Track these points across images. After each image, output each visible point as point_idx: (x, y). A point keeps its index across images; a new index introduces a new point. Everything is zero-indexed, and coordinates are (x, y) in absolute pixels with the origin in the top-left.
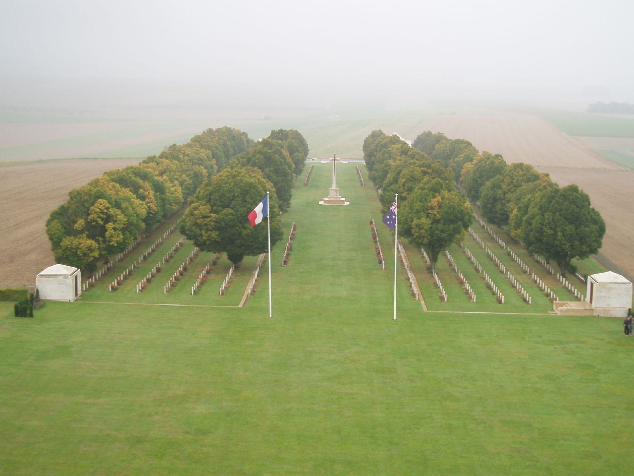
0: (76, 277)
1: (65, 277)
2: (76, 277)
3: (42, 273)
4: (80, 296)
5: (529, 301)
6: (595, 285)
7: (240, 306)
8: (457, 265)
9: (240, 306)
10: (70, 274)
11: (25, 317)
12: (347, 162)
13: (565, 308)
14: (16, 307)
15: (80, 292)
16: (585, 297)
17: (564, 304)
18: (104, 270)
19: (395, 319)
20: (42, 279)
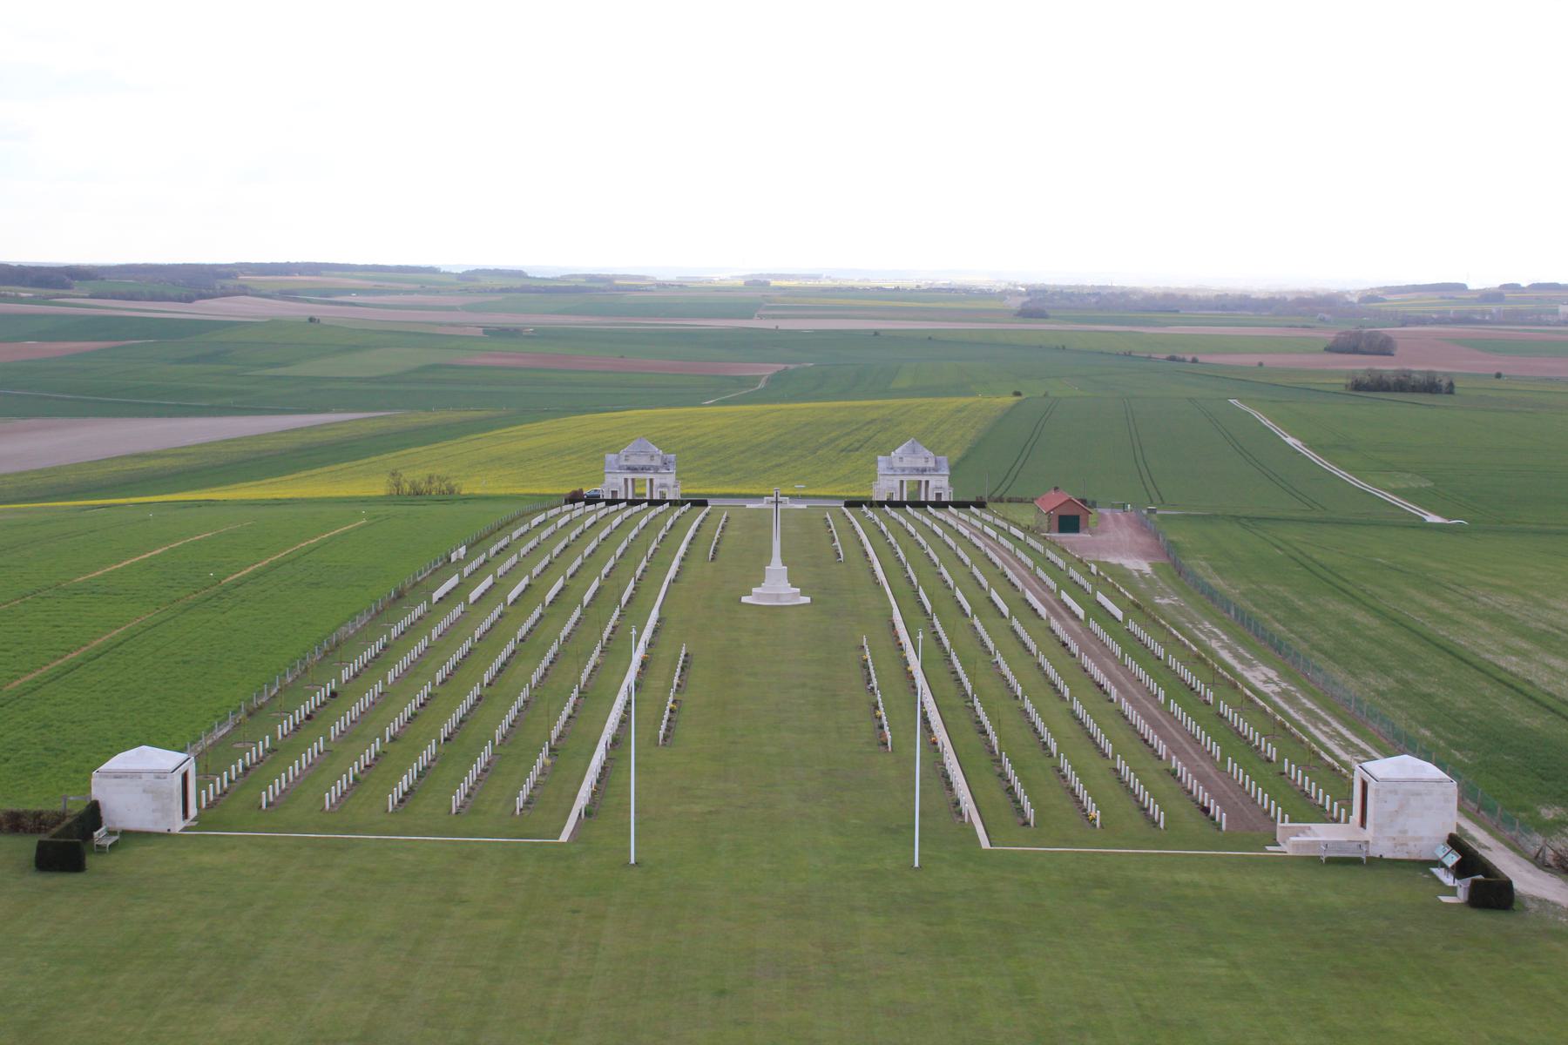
0: (185, 777)
1: (160, 775)
2: (185, 777)
3: (102, 768)
4: (194, 820)
5: (1159, 821)
6: (1372, 785)
7: (564, 838)
8: (1258, 748)
9: (564, 838)
10: (171, 767)
11: (196, 775)
12: (804, 506)
13: (1302, 838)
14: (42, 847)
15: (193, 812)
16: (1349, 813)
17: (1303, 831)
18: (237, 769)
19: (917, 865)
20: (105, 781)
